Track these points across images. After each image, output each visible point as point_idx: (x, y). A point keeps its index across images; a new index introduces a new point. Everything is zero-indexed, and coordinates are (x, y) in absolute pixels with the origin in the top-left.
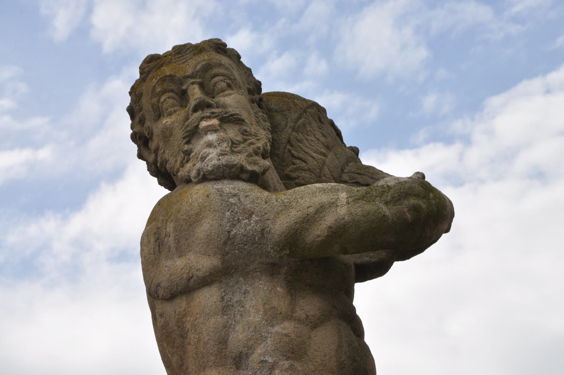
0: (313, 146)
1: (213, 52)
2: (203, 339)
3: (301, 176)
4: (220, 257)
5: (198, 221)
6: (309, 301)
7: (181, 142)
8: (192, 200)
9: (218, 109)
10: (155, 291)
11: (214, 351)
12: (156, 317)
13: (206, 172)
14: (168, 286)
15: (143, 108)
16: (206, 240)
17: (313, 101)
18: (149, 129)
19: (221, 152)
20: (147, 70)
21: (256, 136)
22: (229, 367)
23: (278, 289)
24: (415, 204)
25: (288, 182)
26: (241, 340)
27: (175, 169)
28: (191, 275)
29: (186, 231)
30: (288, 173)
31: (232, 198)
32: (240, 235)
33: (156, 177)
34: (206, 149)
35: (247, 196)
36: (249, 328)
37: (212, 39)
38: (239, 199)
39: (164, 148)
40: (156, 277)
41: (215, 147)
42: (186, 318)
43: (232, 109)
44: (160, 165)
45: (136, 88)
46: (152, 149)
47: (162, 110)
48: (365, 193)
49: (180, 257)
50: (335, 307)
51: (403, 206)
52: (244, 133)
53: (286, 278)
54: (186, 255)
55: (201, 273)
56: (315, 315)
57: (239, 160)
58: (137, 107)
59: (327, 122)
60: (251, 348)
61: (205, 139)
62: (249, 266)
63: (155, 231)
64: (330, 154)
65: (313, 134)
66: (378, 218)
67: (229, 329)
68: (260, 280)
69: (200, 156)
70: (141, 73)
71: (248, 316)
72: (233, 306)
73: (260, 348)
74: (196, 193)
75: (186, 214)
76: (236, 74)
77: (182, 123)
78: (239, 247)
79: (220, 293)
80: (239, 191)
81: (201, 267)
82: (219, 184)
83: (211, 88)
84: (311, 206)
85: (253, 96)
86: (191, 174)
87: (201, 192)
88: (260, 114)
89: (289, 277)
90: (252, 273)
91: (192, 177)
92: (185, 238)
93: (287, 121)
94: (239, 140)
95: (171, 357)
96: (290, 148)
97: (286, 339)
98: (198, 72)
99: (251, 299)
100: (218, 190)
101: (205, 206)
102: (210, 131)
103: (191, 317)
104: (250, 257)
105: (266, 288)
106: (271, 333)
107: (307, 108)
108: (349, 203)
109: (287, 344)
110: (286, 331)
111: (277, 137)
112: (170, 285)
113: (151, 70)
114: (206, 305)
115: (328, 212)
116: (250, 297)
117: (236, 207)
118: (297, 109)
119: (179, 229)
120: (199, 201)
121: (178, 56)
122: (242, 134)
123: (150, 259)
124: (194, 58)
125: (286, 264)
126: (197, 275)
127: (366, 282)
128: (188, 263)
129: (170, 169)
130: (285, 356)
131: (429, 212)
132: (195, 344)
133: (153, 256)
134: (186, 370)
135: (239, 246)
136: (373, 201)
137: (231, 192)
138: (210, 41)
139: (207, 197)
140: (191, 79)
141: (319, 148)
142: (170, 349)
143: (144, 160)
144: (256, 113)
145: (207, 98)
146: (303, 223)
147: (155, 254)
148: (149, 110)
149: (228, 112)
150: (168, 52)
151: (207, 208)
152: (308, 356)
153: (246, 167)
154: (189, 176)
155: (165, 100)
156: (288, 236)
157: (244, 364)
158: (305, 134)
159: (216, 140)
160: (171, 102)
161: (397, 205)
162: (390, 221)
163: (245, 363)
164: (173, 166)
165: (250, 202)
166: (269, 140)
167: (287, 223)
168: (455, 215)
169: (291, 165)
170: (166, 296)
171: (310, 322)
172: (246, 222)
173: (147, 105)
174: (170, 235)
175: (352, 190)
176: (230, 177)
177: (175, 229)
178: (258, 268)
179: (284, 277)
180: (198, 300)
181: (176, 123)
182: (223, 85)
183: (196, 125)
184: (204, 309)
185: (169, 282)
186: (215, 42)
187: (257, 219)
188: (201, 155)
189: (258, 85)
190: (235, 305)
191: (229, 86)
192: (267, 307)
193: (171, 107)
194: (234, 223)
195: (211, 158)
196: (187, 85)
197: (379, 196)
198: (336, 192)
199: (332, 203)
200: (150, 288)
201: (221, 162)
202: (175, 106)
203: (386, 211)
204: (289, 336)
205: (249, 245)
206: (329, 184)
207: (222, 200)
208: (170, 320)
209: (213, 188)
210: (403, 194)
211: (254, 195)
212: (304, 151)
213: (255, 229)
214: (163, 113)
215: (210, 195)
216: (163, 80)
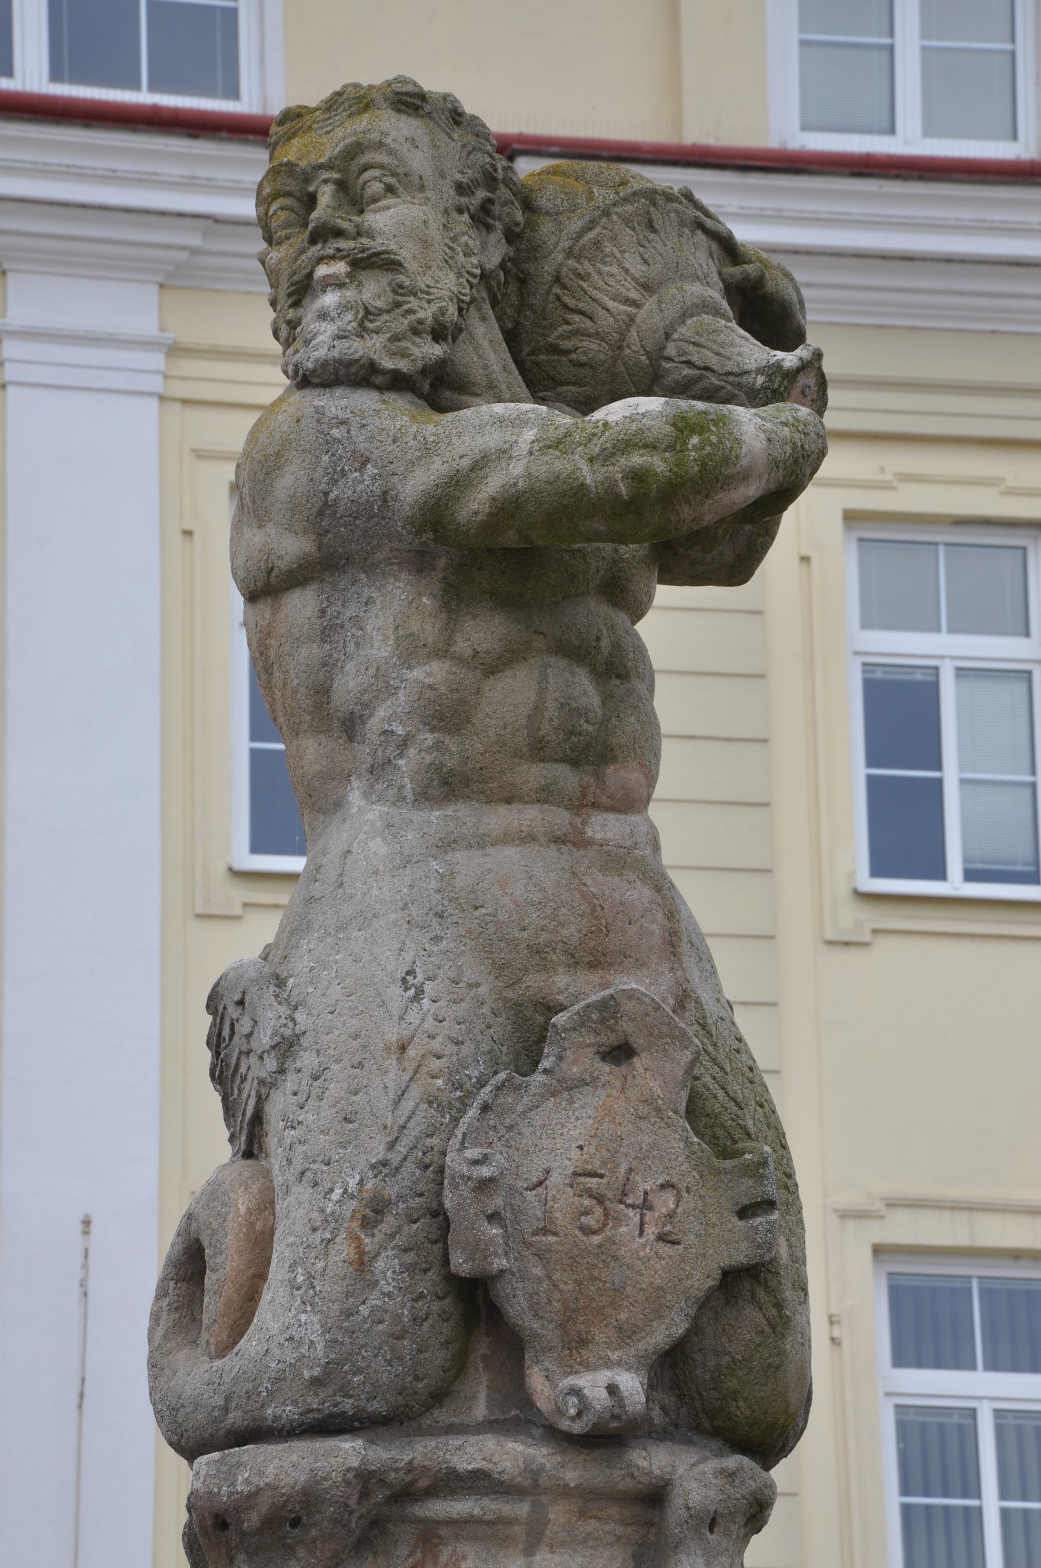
4: (313, 537)
11: (308, 705)
21: (427, 294)
23: (424, 599)
28: (271, 566)
30: (553, 342)
31: (338, 427)
35: (364, 426)
38: (348, 432)
41: (333, 320)
53: (445, 578)
64: (650, 299)
66: (571, 489)
68: (397, 579)
71: (369, 645)
72: (342, 626)
75: (261, 450)
79: (318, 602)
81: (283, 553)
89: (450, 577)
96: (559, 291)
97: (430, 694)
100: (318, 410)
106: (406, 680)
107: (614, 205)
110: (431, 679)
117: (341, 447)
122: (394, 291)
130: (428, 724)
141: (624, 290)
146: (449, 487)
152: (473, 725)
153: (380, 364)
155: (275, 213)
169: (562, 324)
172: (356, 477)
176: (350, 381)
179: (441, 576)
180: (285, 611)
182: (377, 187)
184: (291, 628)
190: (348, 624)
191: (390, 190)
192: (401, 633)
194: (335, 476)
195: (318, 343)
202: (290, 226)
203: (588, 475)
205: (364, 519)
207: (318, 431)
212: (590, 297)
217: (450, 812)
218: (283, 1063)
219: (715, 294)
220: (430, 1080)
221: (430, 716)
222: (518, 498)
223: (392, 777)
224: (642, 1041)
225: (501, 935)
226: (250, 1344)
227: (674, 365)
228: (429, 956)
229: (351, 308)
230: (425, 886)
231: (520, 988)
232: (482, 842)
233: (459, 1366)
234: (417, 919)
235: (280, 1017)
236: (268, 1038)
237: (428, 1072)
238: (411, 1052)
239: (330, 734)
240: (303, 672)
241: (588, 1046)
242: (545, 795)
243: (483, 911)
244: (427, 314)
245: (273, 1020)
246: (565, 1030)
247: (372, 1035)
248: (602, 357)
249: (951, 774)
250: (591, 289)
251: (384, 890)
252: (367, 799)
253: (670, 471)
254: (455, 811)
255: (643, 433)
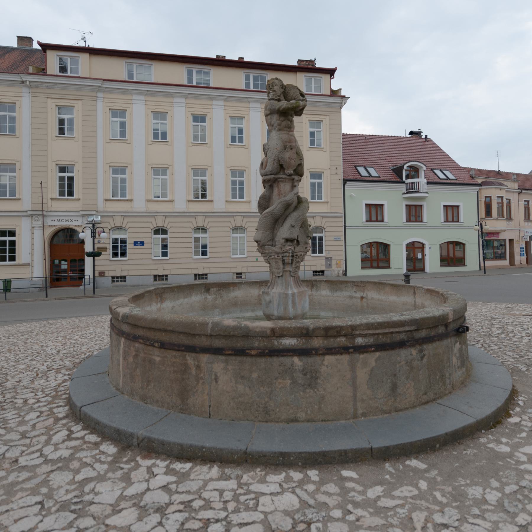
219: (299, 94)
226: (266, 169)
232: (282, 134)
233: (280, 171)
242: (286, 131)
244: (278, 95)
249: (315, 139)
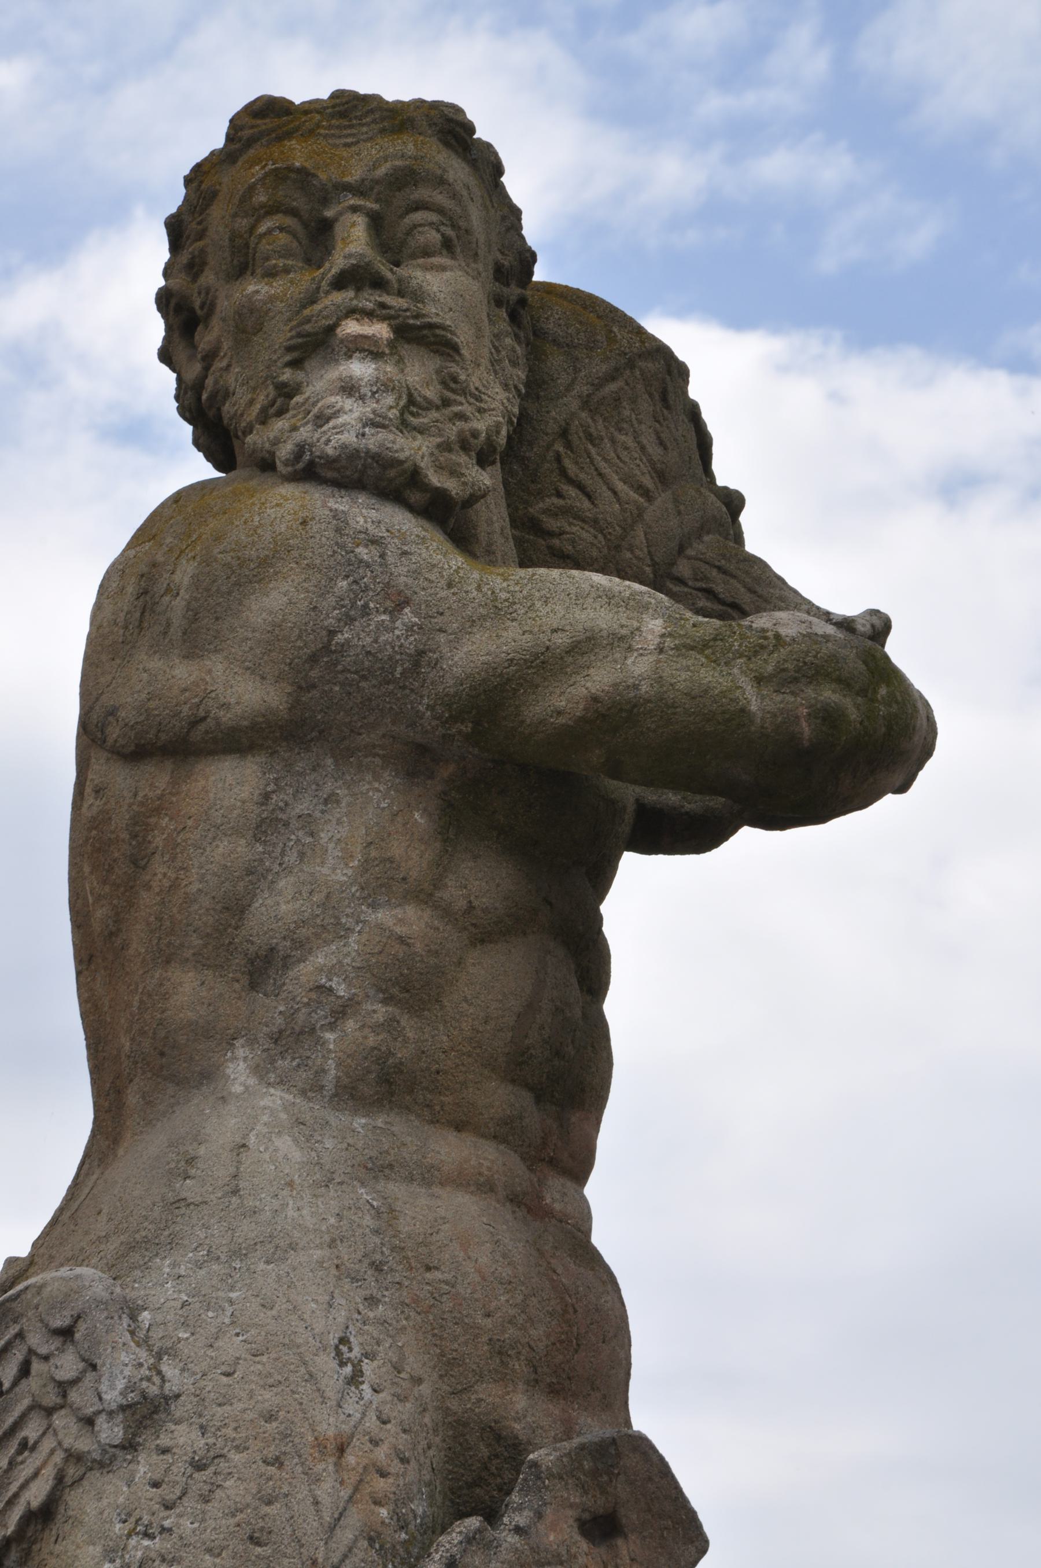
0: (624, 463)
1: (434, 139)
2: (186, 885)
3: (568, 533)
4: (289, 689)
5: (261, 580)
6: (486, 869)
7: (279, 358)
8: (261, 519)
9: (400, 300)
10: (100, 725)
12: (84, 790)
13: (320, 457)
14: (137, 723)
15: (208, 234)
16: (268, 635)
17: (660, 341)
18: (207, 293)
19: (372, 416)
20: (247, 133)
21: (477, 400)
22: (231, 975)
23: (417, 816)
24: (833, 704)
25: (532, 537)
26: (282, 918)
27: (243, 424)
28: (203, 714)
29: (222, 597)
31: (366, 546)
32: (359, 650)
33: (190, 423)
34: (338, 397)
35: (405, 553)
36: (310, 893)
37: (442, 102)
38: (382, 556)
39: (231, 358)
40: (114, 688)
41: (362, 398)
42: (159, 818)
43: (437, 309)
44: (209, 398)
45: (205, 173)
46: (200, 349)
47: (254, 255)
48: (712, 636)
49: (188, 657)
50: (550, 904)
51: (799, 699)
52: (450, 382)
53: (445, 793)
54: (205, 658)
55: (229, 715)
56: (492, 910)
57: (412, 452)
58: (194, 225)
59: (682, 407)
60: (302, 947)
61: (341, 368)
62: (360, 734)
63: (145, 570)
64: (663, 495)
65: (635, 431)
66: (724, 712)
67: (260, 881)
68: (377, 777)
69: (315, 410)
70: (230, 138)
71: (318, 860)
72: (287, 824)
73: (324, 953)
74: (277, 505)
75: (233, 550)
76: (476, 217)
77: (296, 306)
78: (347, 678)
80: (389, 534)
81: (233, 701)
82: (344, 500)
83: (399, 235)
84: (562, 630)
85: (505, 289)
86: (279, 449)
87: (291, 505)
88: (508, 341)
90: (360, 754)
91: (279, 459)
92: (215, 612)
93: (576, 378)
94: (431, 397)
95: (93, 904)
96: (561, 449)
97: (400, 951)
98: (377, 182)
99: (338, 820)
100: (335, 514)
101: (290, 546)
102: (361, 351)
103: (171, 819)
104: (367, 713)
105: (386, 805)
106: (364, 922)
107: (640, 356)
108: (664, 650)
109: (397, 962)
110: (404, 929)
111: (535, 411)
112: (143, 721)
113: (258, 139)
114: (218, 802)
115: (601, 657)
116: (338, 816)
117: (369, 574)
118: (611, 351)
119: (205, 584)
120: (278, 529)
121: (337, 123)
122: (444, 383)
123: (110, 638)
124: (379, 141)
125: (456, 758)
126: (217, 719)
127: (653, 857)
128: (203, 680)
129: (231, 419)
130: (383, 991)
131: (862, 732)
132: (161, 890)
133: (121, 632)
134: (123, 948)
135: (348, 676)
136: (725, 663)
137: (367, 529)
138: (436, 105)
139: (301, 524)
140: (354, 195)
142: (95, 884)
143: (174, 370)
144: (497, 336)
145: (380, 261)
146: (528, 668)
147: (126, 627)
148: (221, 242)
149: (424, 316)
150: (317, 101)
151: (292, 552)
152: (442, 1007)
153: (426, 476)
154: (273, 454)
155: (269, 231)
156: (482, 689)
157: (272, 981)
158: (613, 424)
159: (369, 380)
160: (282, 242)
161: (784, 693)
162: (753, 729)
163: (275, 979)
164: (239, 412)
165: (409, 571)
166: (510, 419)
167: (487, 654)
168: (935, 753)
169: (552, 495)
170: (123, 746)
171: (473, 924)
172: (383, 621)
173: (221, 229)
174: (178, 594)
175: (681, 619)
177: (196, 581)
178: (380, 746)
180: (203, 782)
181: (281, 302)
182: (433, 237)
183: (329, 325)
185: (141, 715)
186: (446, 115)
187: (413, 620)
188: (320, 409)
189: (528, 257)
190: (294, 824)
191: (447, 245)
192: (374, 853)
193: (280, 257)
194: (352, 613)
195: (343, 425)
196: (339, 208)
197: (746, 656)
198: (640, 610)
199: (619, 636)
200: (89, 712)
201: (366, 444)
202: (291, 255)
204: (408, 945)
205: (374, 682)
206: (627, 583)
207: (337, 544)
208: (117, 811)
209: (324, 505)
210: (810, 668)
211: (424, 555)
212: (596, 469)
213: (402, 644)
214: (253, 265)
215: (311, 520)
216: (280, 176)
217: (380, 1123)
218: (134, 1435)
220: (373, 1506)
221: (390, 980)
222: (635, 706)
223: (309, 1054)
224: (635, 1517)
225: (459, 1315)
227: (686, 590)
228: (364, 1323)
229: (393, 389)
230: (357, 1219)
231: (470, 1398)
234: (347, 1264)
235: (141, 1365)
236: (116, 1393)
237: (370, 1493)
238: (350, 1459)
239: (223, 973)
240: (215, 874)
241: (571, 1506)
243: (438, 1275)
245: (129, 1368)
246: (551, 1476)
247: (296, 1420)
248: (595, 553)
250: (600, 459)
251: (304, 1212)
252: (261, 1078)
253: (861, 723)
254: (387, 1123)
255: (837, 662)
